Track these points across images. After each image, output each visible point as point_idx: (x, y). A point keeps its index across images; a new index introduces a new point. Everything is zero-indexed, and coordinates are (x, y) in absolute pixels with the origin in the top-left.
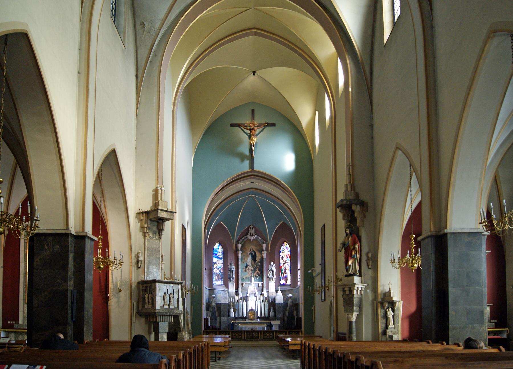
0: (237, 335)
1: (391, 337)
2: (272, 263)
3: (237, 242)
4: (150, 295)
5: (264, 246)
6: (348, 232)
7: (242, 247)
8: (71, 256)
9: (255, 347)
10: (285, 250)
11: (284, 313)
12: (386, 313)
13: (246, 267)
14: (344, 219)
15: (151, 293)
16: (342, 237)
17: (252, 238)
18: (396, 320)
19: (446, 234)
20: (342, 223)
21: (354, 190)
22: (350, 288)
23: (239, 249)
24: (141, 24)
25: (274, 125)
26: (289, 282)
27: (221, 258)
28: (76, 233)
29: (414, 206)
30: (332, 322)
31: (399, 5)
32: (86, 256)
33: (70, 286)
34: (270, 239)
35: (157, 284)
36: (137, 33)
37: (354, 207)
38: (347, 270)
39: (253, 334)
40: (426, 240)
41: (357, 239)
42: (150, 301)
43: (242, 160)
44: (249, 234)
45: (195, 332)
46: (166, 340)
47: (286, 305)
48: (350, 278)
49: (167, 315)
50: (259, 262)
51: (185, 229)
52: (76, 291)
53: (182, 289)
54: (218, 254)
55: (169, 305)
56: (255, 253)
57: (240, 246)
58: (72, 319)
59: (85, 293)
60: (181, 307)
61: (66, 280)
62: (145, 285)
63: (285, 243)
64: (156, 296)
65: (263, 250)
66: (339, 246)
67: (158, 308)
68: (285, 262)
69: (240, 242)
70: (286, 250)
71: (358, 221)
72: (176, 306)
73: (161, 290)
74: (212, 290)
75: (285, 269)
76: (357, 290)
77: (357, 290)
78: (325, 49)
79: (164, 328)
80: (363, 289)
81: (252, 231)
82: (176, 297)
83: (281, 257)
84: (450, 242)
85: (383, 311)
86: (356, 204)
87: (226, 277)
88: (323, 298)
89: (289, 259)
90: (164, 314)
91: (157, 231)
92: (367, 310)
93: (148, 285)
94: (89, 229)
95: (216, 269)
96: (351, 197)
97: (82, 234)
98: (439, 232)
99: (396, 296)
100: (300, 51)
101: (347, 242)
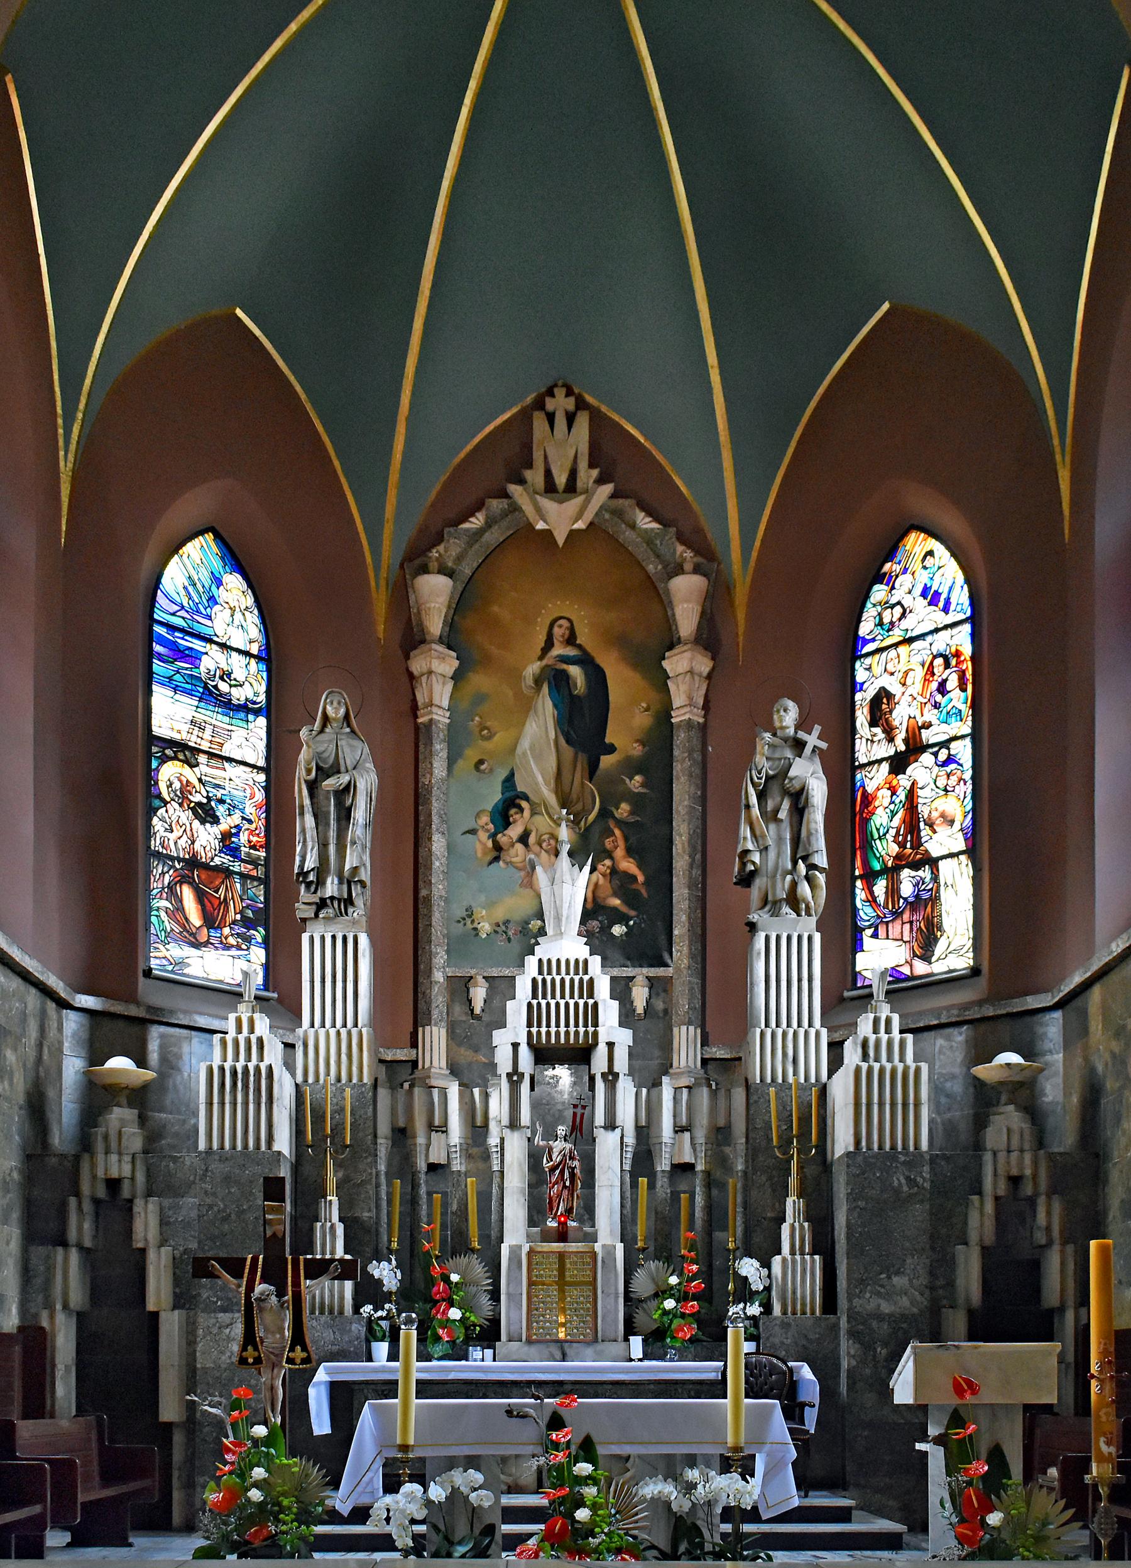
2: (789, 716)
5: (686, 594)
7: (461, 605)
10: (922, 611)
11: (942, 1268)
13: (503, 817)
17: (560, 518)
23: (435, 625)
26: (955, 952)
27: (246, 709)
29: (787, 886)
31: (715, 391)
44: (535, 476)
47: (958, 1161)
50: (632, 767)
54: (212, 660)
57: (435, 592)
63: (916, 544)
68: (915, 748)
69: (448, 550)
70: (923, 617)
81: (564, 447)
83: (862, 699)
89: (958, 699)
95: (176, 813)
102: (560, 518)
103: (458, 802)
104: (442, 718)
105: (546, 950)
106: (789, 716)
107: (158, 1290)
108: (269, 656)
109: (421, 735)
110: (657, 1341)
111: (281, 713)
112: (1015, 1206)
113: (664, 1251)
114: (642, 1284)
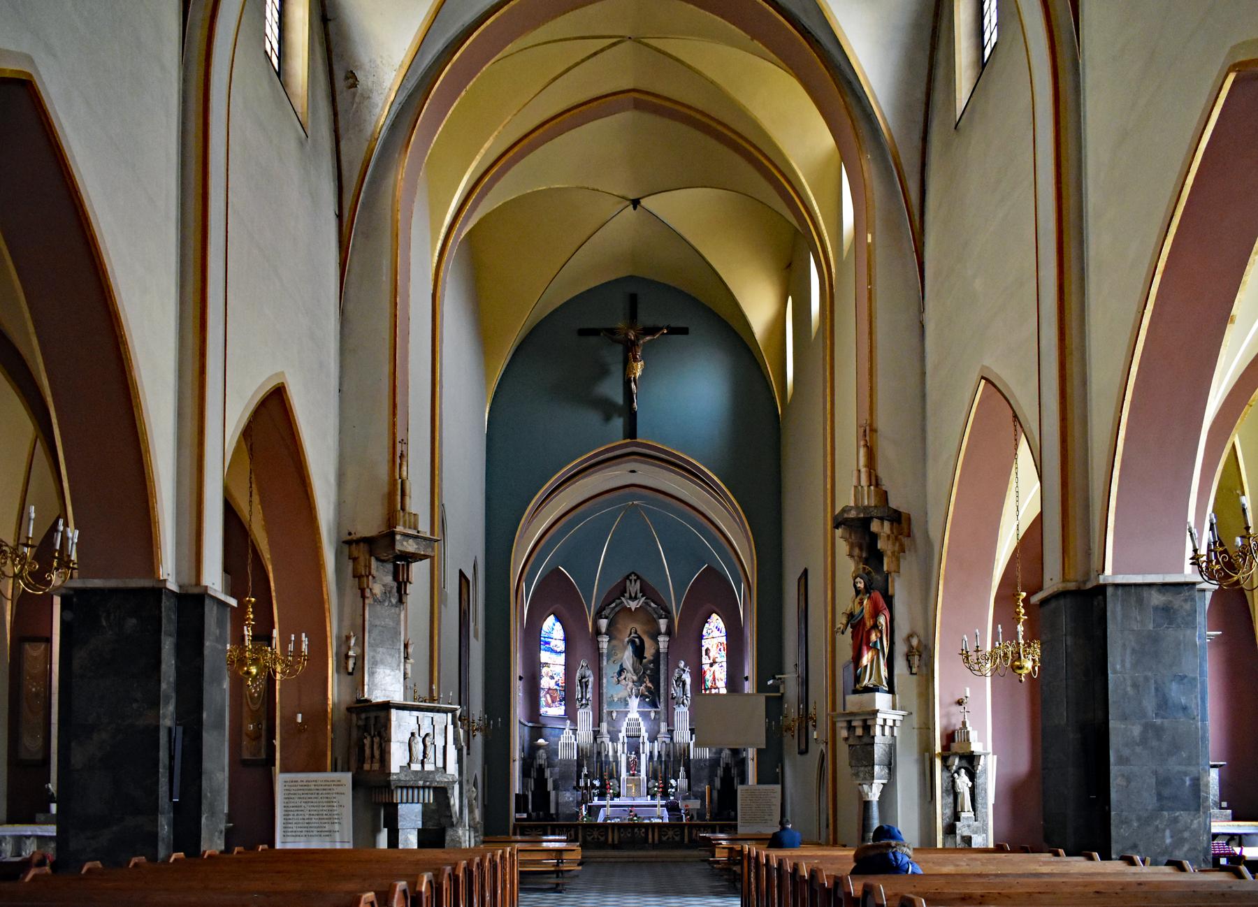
0: (596, 834)
1: (968, 840)
2: (682, 664)
3: (599, 615)
4: (377, 740)
5: (663, 624)
6: (861, 585)
7: (609, 625)
8: (168, 646)
9: (637, 862)
10: (715, 633)
12: (954, 781)
13: (620, 674)
14: (851, 555)
15: (380, 735)
16: (846, 600)
18: (979, 800)
19: (1104, 586)
20: (847, 566)
21: (877, 485)
22: (865, 721)
23: (604, 630)
24: (347, 78)
25: (684, 331)
28: (180, 587)
30: (823, 805)
32: (207, 644)
33: (165, 717)
34: (677, 605)
35: (393, 711)
36: (338, 98)
37: (875, 526)
38: (858, 679)
39: (633, 833)
40: (1053, 604)
41: (882, 603)
42: (377, 753)
43: (608, 418)
44: (627, 595)
45: (493, 827)
46: (415, 847)
48: (866, 696)
49: (418, 788)
50: (651, 662)
51: (468, 581)
52: (180, 729)
53: (454, 723)
54: (553, 643)
55: (423, 763)
56: (642, 641)
57: (603, 623)
58: (171, 798)
59: (204, 734)
60: (452, 768)
61: (154, 702)
62: (363, 716)
63: (714, 616)
64: (389, 741)
65: (660, 633)
66: (841, 620)
67: (395, 768)
70: (716, 633)
71: (886, 561)
72: (440, 764)
73: (402, 725)
74: (537, 726)
75: (714, 679)
76: (883, 727)
77: (883, 727)
78: (803, 136)
79: (410, 818)
80: (898, 723)
81: (634, 587)
82: (440, 742)
84: (1114, 608)
85: (947, 774)
86: (882, 519)
87: (568, 697)
88: (803, 747)
89: (724, 653)
90: (411, 783)
91: (395, 585)
92: (907, 773)
93: (372, 715)
94: (213, 578)
96: (869, 500)
97: (196, 591)
98: (1085, 582)
99: (981, 742)
100: (747, 146)
101: (857, 610)
102: (633, 605)
103: (609, 670)
104: (605, 651)
105: (630, 716)
106: (682, 664)
107: (550, 786)
108: (566, 640)
109: (600, 655)
110: (653, 797)
111: (568, 651)
112: (727, 769)
113: (655, 778)
114: (650, 785)
